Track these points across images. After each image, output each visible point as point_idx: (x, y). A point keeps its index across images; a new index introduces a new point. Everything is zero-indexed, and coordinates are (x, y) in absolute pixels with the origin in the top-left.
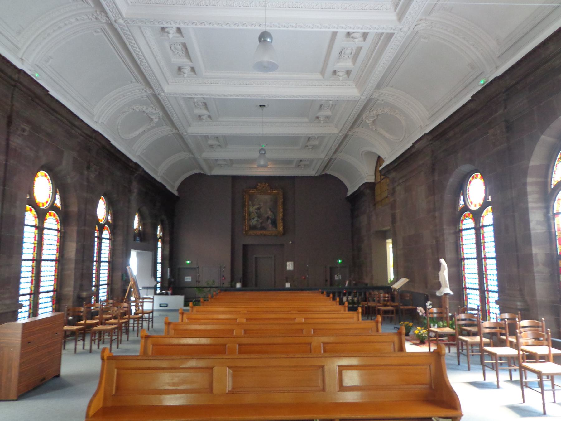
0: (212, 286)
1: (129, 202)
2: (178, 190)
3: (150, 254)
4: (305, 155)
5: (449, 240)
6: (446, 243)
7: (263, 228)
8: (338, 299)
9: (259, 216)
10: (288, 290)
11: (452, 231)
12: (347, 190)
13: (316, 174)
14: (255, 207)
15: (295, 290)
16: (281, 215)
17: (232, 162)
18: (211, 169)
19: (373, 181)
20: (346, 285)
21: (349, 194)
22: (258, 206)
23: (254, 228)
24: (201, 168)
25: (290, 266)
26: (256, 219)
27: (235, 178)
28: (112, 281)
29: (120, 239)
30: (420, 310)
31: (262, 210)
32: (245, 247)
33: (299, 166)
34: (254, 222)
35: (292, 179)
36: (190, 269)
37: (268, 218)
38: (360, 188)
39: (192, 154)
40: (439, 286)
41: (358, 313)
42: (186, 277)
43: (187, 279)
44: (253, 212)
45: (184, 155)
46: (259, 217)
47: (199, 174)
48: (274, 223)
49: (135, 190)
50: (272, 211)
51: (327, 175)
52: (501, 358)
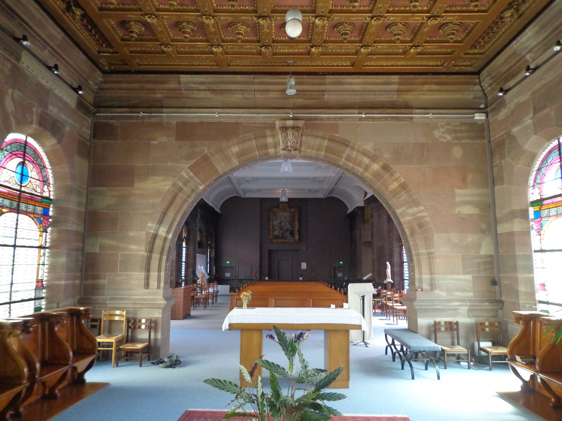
0: (248, 279)
1: (196, 223)
2: (221, 209)
3: (205, 256)
4: (315, 186)
5: (396, 250)
6: (394, 252)
7: (284, 237)
8: (333, 287)
9: (281, 228)
10: (301, 281)
11: (398, 245)
12: (347, 209)
13: (323, 196)
14: (277, 222)
15: (305, 281)
16: (297, 227)
17: (260, 190)
18: (245, 193)
19: (363, 205)
20: (532, 322)
21: (349, 212)
22: (280, 221)
23: (277, 237)
24: (237, 193)
25: (304, 266)
26: (278, 230)
27: (262, 199)
28: (187, 275)
29: (191, 247)
30: (389, 296)
31: (283, 224)
32: (270, 251)
33: (314, 181)
34: (276, 233)
35: (306, 200)
36: (230, 267)
37: (287, 230)
38: (354, 209)
39: (234, 185)
40: (385, 277)
41: (332, 289)
42: (226, 274)
43: (227, 275)
44: (276, 225)
45: (228, 186)
46: (280, 229)
47: (236, 197)
48: (292, 234)
49: (199, 215)
50: (290, 225)
51: (332, 197)
52: (399, 310)
